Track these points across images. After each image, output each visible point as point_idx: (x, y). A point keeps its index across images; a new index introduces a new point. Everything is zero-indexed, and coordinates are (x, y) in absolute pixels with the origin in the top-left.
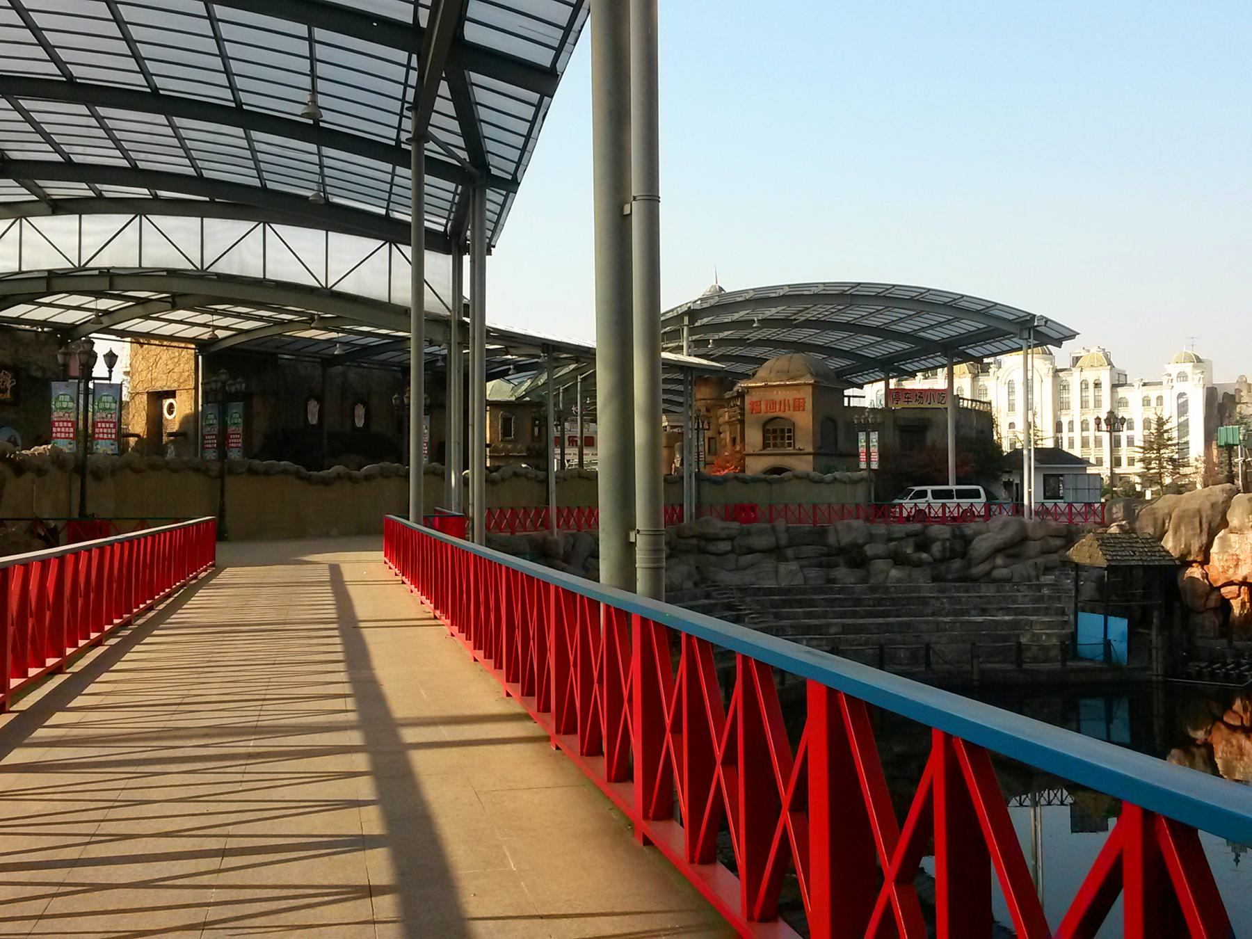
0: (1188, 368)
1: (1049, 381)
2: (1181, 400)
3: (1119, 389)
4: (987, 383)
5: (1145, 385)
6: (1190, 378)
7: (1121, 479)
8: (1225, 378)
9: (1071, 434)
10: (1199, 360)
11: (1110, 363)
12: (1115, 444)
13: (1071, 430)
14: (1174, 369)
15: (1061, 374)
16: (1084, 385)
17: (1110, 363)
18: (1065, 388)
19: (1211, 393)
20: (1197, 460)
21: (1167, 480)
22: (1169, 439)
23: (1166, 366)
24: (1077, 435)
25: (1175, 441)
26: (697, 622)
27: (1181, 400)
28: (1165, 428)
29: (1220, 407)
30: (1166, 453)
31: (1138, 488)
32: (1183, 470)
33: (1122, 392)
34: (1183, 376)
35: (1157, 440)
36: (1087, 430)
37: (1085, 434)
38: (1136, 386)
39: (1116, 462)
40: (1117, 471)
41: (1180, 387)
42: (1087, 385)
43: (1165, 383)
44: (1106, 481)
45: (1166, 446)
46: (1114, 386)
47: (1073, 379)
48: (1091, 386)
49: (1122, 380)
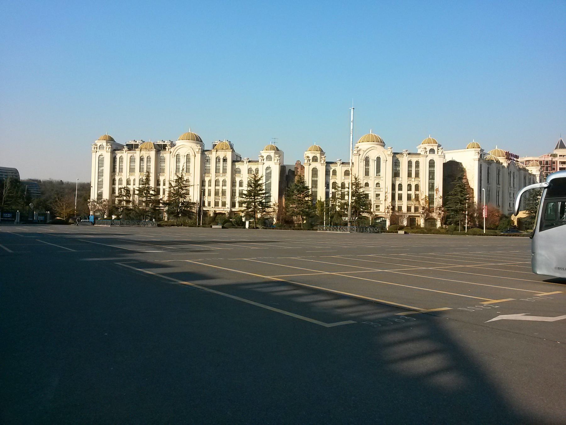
0: (272, 153)
1: (199, 156)
2: (268, 171)
3: (236, 163)
4: (164, 155)
5: (249, 162)
6: (273, 159)
7: (235, 214)
8: (290, 162)
9: (210, 188)
10: (278, 150)
11: (232, 148)
12: (235, 172)
13: (210, 185)
14: (265, 154)
15: (206, 153)
16: (218, 159)
17: (232, 148)
18: (208, 161)
19: (283, 169)
20: (274, 205)
21: (259, 216)
22: (261, 190)
23: (261, 152)
24: (212, 199)
25: (264, 192)
26: (52, 231)
27: (268, 171)
28: (260, 182)
29: (289, 177)
30: (259, 199)
31: (244, 219)
32: (267, 210)
33: (238, 165)
34: (269, 158)
35: (255, 184)
36: (219, 185)
37: (217, 188)
38: (245, 162)
39: (233, 205)
40: (233, 210)
41: (267, 164)
42: (219, 159)
43: (260, 161)
44: (227, 215)
45: (259, 195)
46: (234, 162)
47: (213, 156)
48: (221, 160)
49: (239, 159)
